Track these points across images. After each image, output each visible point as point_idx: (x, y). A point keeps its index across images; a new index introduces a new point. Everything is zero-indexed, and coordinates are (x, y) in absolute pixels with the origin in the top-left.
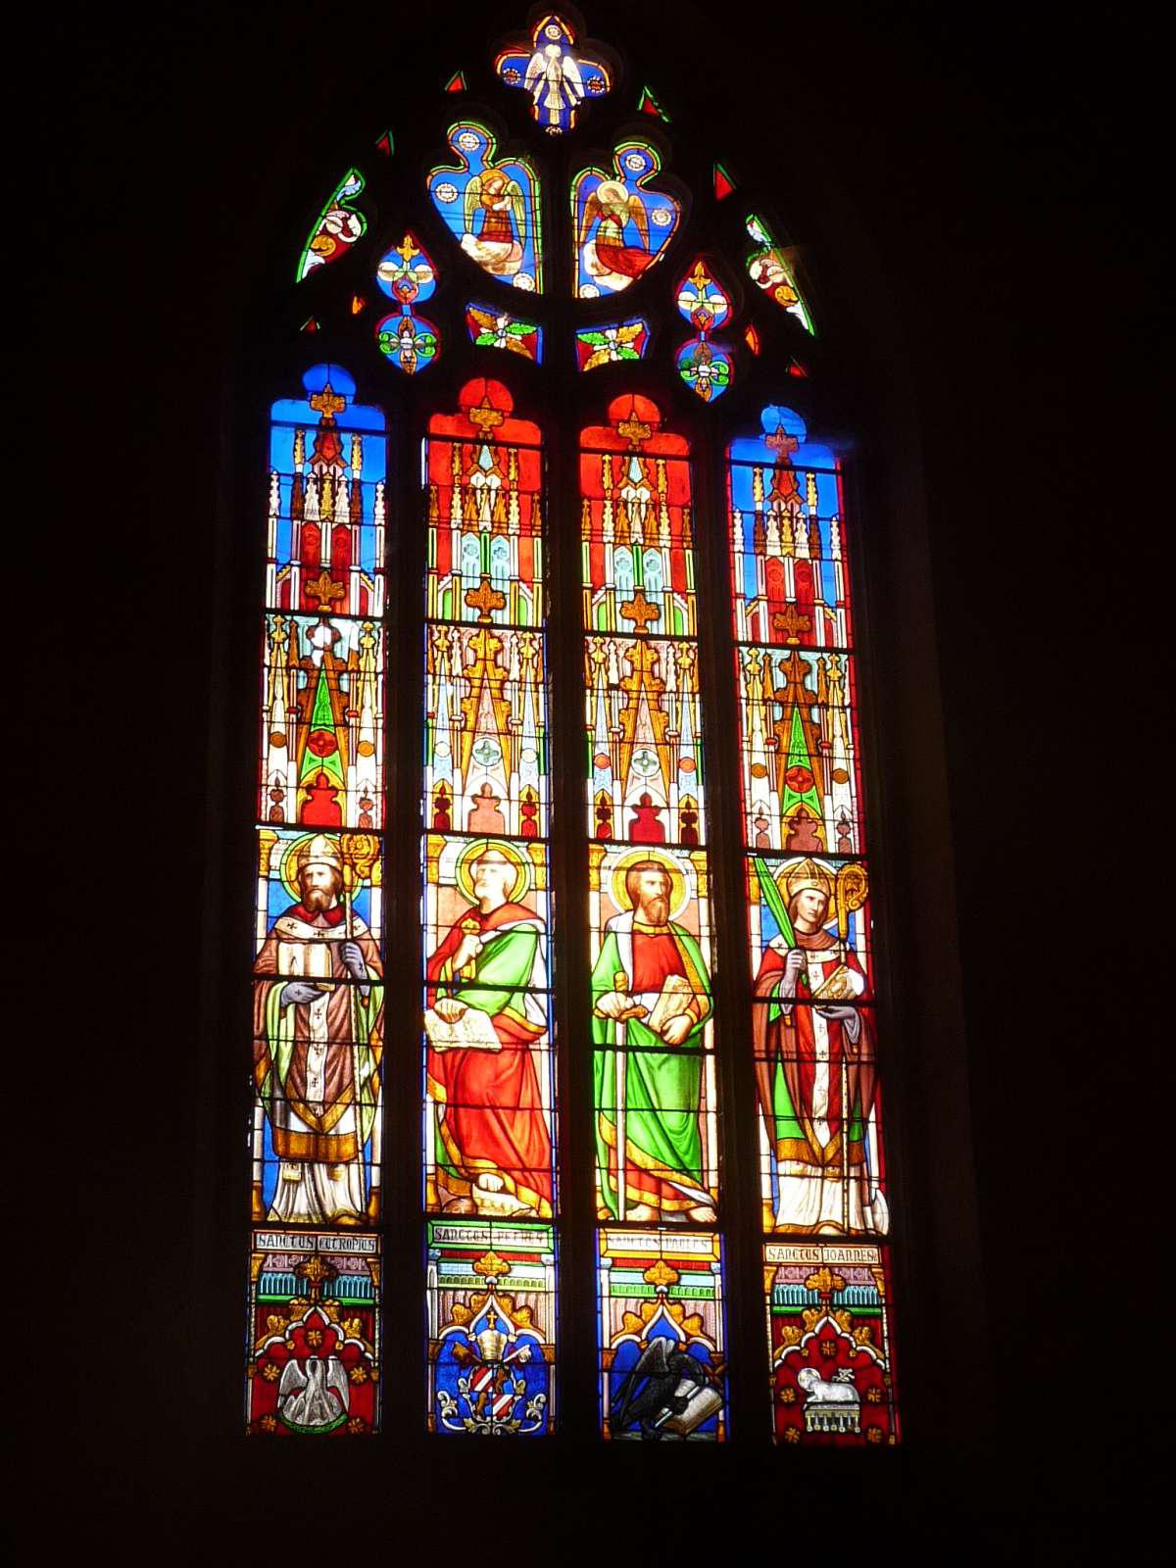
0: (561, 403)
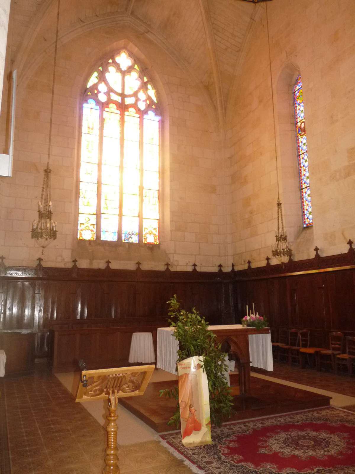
0: (123, 107)
